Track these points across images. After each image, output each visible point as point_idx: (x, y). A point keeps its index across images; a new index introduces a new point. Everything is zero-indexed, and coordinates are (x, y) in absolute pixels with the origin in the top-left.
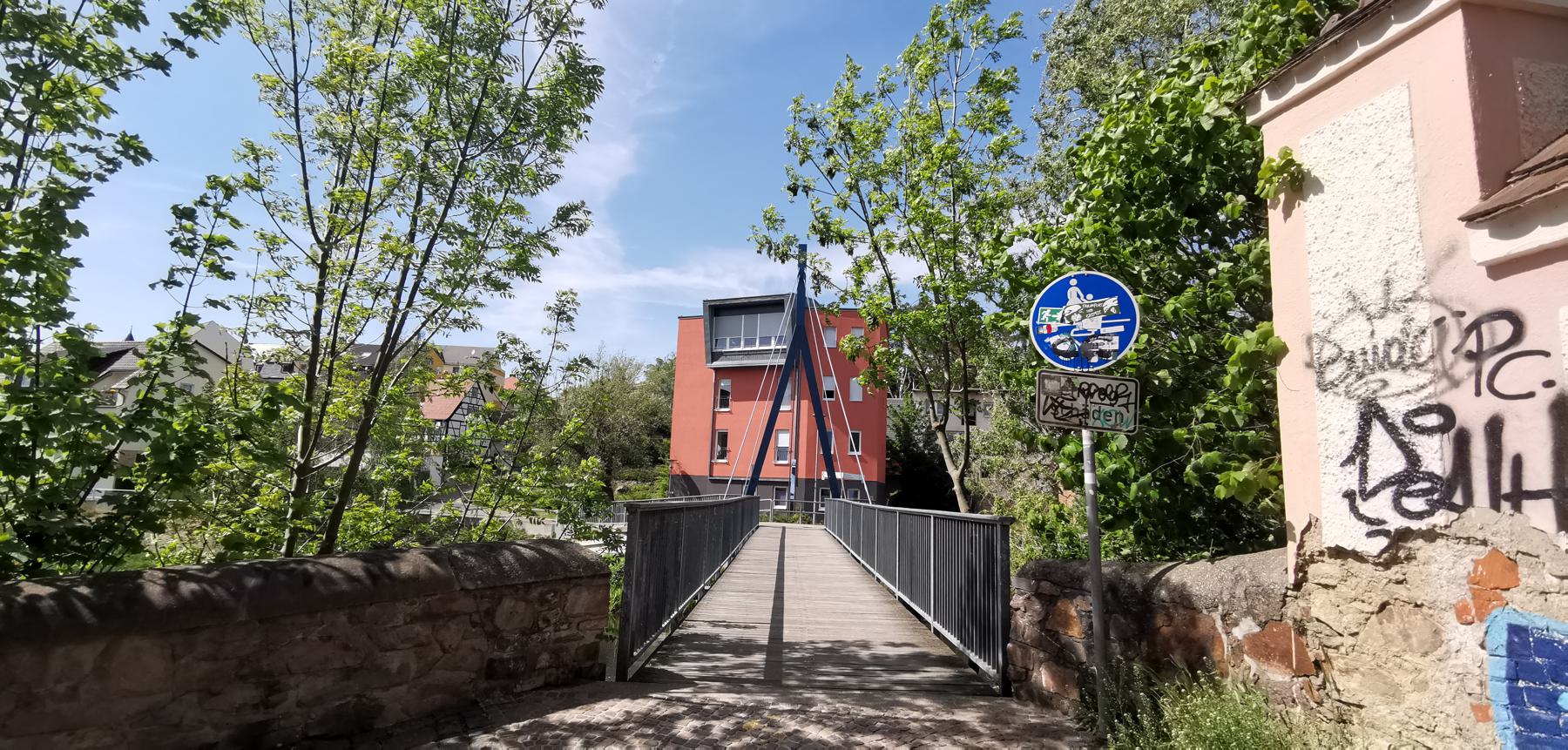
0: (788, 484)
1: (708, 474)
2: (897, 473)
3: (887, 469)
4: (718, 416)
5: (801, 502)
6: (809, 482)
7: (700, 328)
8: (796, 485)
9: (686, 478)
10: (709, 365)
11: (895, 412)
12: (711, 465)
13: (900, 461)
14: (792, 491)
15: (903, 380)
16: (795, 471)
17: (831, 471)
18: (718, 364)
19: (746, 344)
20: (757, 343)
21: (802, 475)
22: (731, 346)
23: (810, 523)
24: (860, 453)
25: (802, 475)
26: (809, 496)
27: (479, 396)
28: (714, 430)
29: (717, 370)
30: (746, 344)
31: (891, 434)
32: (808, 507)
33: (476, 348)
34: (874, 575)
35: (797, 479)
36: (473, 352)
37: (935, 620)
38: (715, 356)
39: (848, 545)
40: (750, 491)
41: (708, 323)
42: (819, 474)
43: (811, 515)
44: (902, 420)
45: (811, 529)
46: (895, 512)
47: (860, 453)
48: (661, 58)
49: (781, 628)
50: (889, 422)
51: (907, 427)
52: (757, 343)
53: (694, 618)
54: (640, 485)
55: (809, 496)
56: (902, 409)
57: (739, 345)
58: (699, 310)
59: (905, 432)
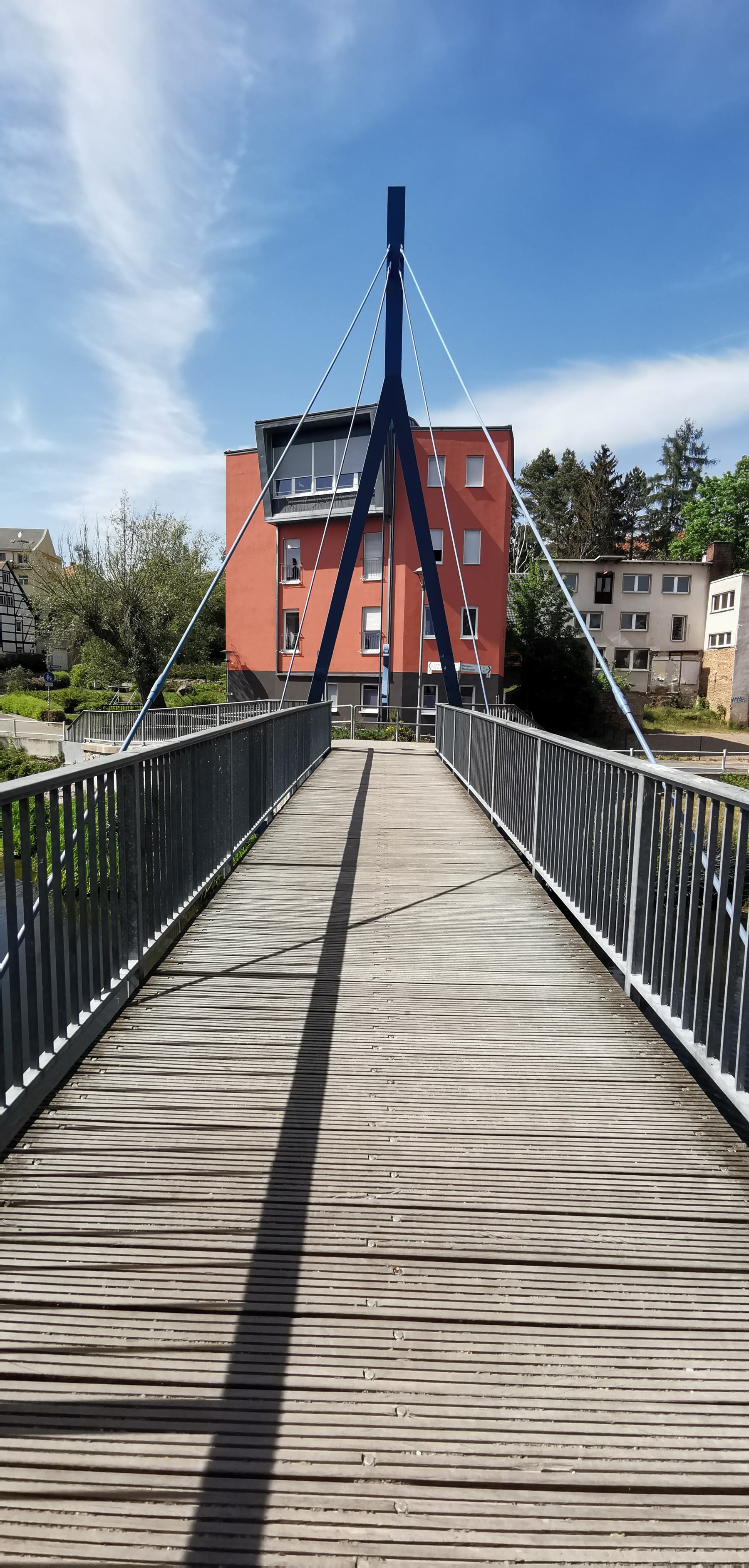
0: (379, 680)
1: (275, 669)
2: (517, 664)
3: (506, 660)
4: (285, 590)
5: (396, 708)
6: (409, 678)
7: (254, 464)
8: (391, 681)
9: (249, 675)
10: (269, 519)
11: (517, 585)
12: (279, 657)
13: (522, 649)
14: (385, 690)
15: (519, 552)
16: (388, 662)
17: (447, 661)
18: (282, 517)
19: (319, 487)
20: (334, 483)
21: (398, 667)
22: (299, 489)
23: (411, 739)
24: (476, 638)
25: (398, 667)
26: (409, 699)
27: (12, 581)
28: (280, 610)
29: (281, 526)
30: (319, 487)
31: (512, 615)
32: (409, 716)
33: (23, 531)
34: (489, 816)
35: (391, 675)
36: (20, 535)
37: (494, 811)
38: (276, 506)
39: (489, 801)
40: (315, 695)
41: (264, 457)
42: (425, 666)
43: (414, 728)
44: (526, 596)
45: (406, 753)
46: (453, 710)
47: (476, 638)
48: (231, 167)
49: (356, 854)
50: (510, 600)
51: (532, 605)
52: (334, 483)
53: (130, 1014)
54: (209, 684)
55: (409, 699)
56: (526, 581)
57: (308, 488)
58: (250, 441)
59: (528, 611)
